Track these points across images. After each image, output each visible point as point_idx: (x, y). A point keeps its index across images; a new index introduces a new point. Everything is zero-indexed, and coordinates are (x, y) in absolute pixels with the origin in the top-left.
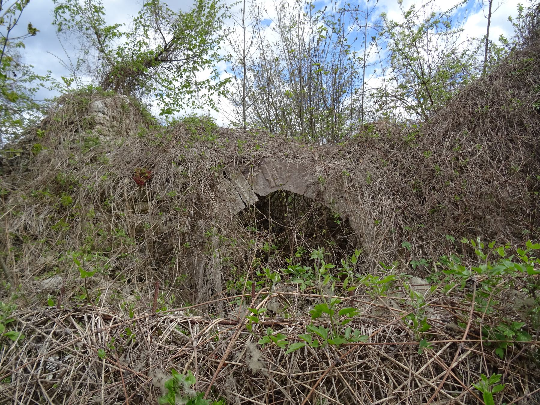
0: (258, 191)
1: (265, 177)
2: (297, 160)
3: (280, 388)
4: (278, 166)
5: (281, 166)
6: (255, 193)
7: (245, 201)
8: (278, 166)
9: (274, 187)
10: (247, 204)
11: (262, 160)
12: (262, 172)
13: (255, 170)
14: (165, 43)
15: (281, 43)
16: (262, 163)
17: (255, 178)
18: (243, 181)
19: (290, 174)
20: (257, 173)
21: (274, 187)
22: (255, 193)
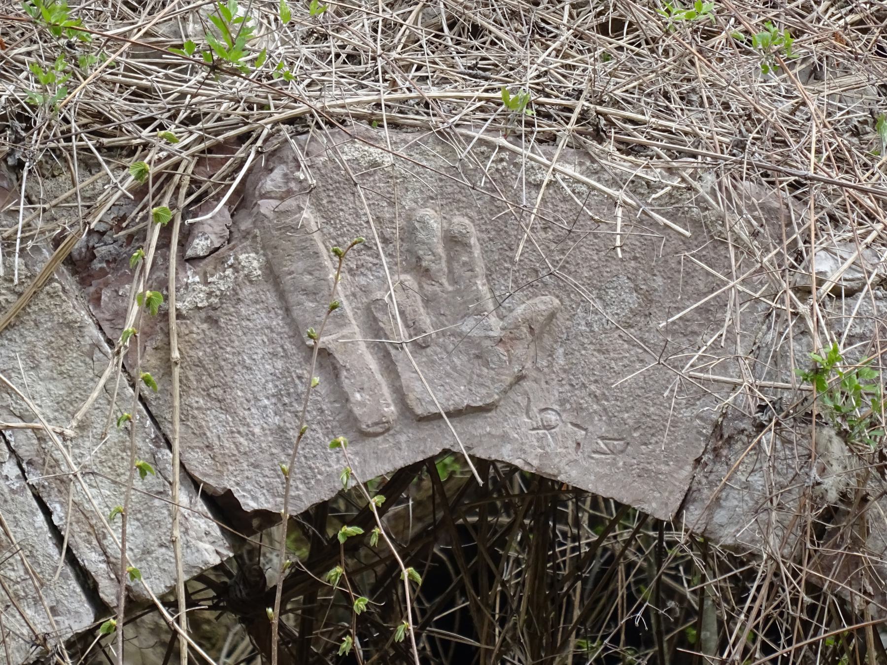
0: (219, 462)
1: (295, 329)
2: (623, 165)
3: (343, 56)
4: (431, 216)
5: (461, 222)
6: (193, 482)
7: (91, 559)
8: (431, 216)
9: (385, 429)
10: (108, 592)
11: (274, 156)
12: (272, 275)
13: (199, 246)
14: (678, 515)
15: (304, 537)
16: (273, 181)
17: (199, 327)
18: (73, 361)
19: (545, 302)
20: (222, 280)
21: (385, 429)
22: (193, 482)
